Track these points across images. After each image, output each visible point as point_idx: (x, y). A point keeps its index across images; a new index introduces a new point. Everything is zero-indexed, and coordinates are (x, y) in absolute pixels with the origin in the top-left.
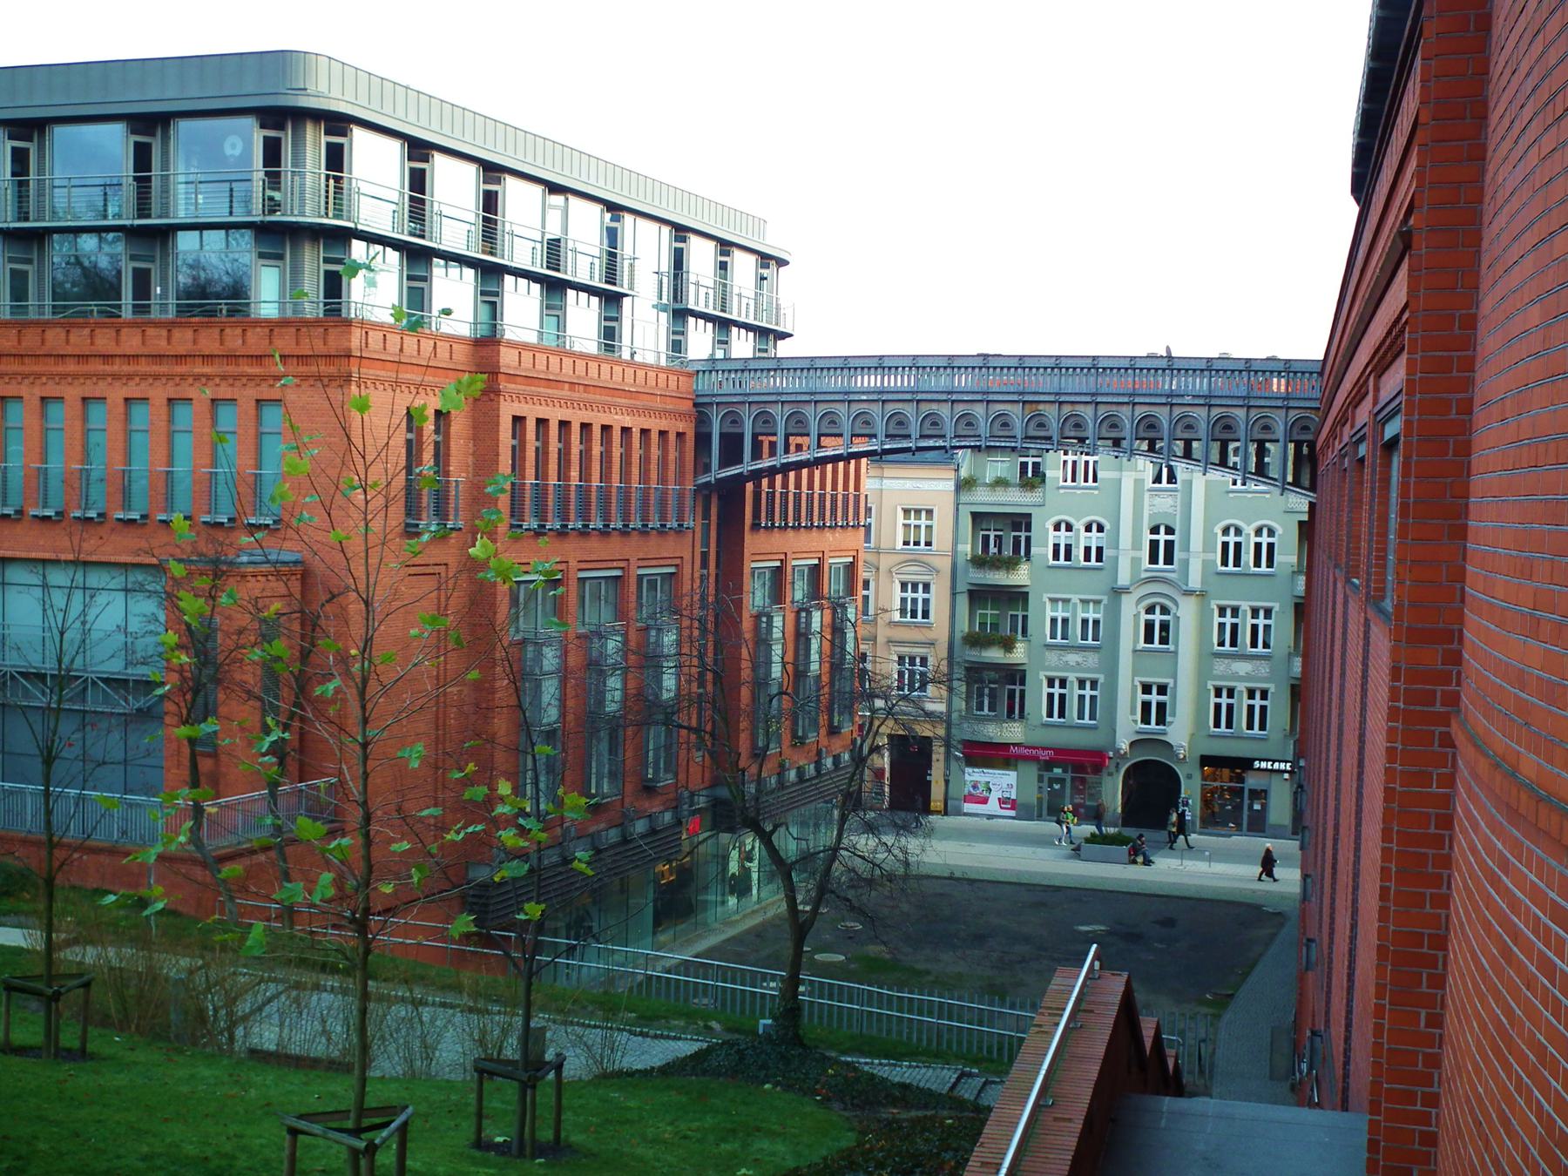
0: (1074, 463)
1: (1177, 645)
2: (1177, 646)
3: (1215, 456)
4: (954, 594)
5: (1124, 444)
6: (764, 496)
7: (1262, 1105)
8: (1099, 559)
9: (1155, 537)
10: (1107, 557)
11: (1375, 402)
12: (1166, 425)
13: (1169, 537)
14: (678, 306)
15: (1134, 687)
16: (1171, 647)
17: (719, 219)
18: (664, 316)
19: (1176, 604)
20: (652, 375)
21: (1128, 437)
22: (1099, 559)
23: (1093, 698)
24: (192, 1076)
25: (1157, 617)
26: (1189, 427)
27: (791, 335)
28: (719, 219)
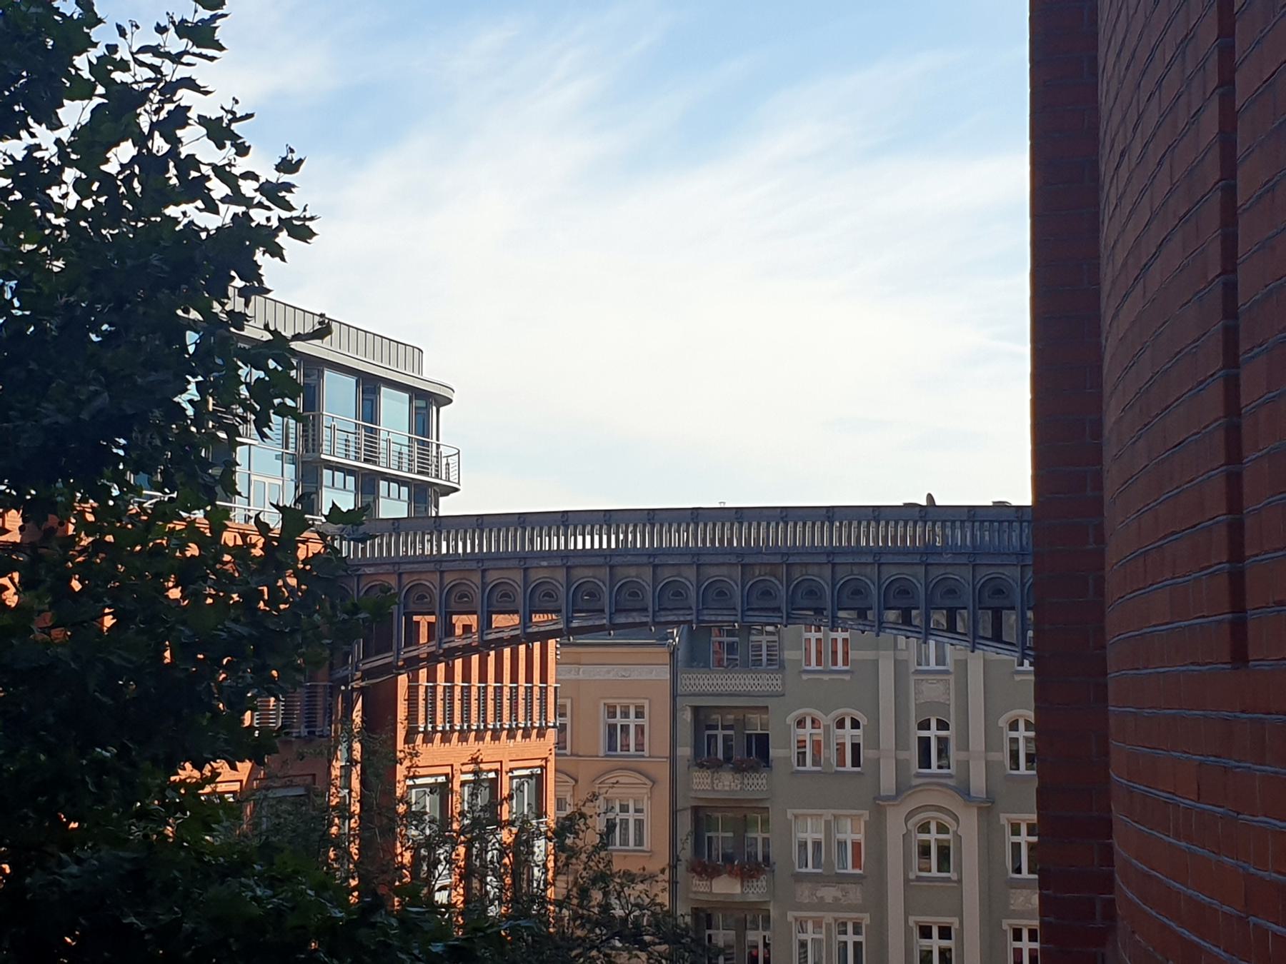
2: (960, 874)
3: (986, 629)
4: (674, 813)
5: (870, 615)
6: (422, 691)
7: (888, 832)
9: (924, 733)
12: (921, 589)
13: (943, 733)
14: (310, 456)
15: (908, 929)
16: (952, 875)
17: (362, 348)
18: (290, 469)
19: (956, 819)
21: (875, 606)
22: (856, 762)
23: (857, 946)
25: (933, 837)
26: (999, 592)
27: (456, 490)
28: (362, 348)
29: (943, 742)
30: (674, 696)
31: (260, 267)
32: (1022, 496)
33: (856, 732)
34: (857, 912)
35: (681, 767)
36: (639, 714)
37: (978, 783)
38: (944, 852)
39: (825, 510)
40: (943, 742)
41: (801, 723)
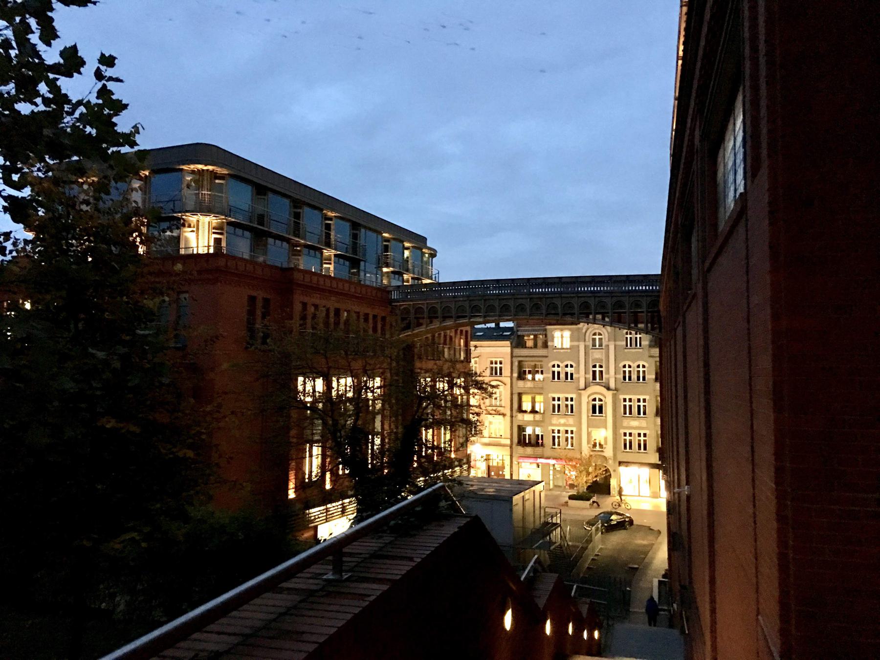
0: (631, 338)
1: (606, 413)
4: (512, 394)
8: (572, 378)
10: (575, 377)
11: (381, 549)
16: (604, 415)
20: (369, 290)
22: (572, 378)
24: (326, 509)
25: (597, 403)
29: (601, 372)
30: (512, 357)
31: (121, 101)
32: (655, 267)
33: (572, 369)
34: (704, 10)
35: (515, 380)
36: (501, 363)
37: (612, 385)
38: (601, 407)
39: (526, 281)
40: (601, 372)
41: (554, 366)
